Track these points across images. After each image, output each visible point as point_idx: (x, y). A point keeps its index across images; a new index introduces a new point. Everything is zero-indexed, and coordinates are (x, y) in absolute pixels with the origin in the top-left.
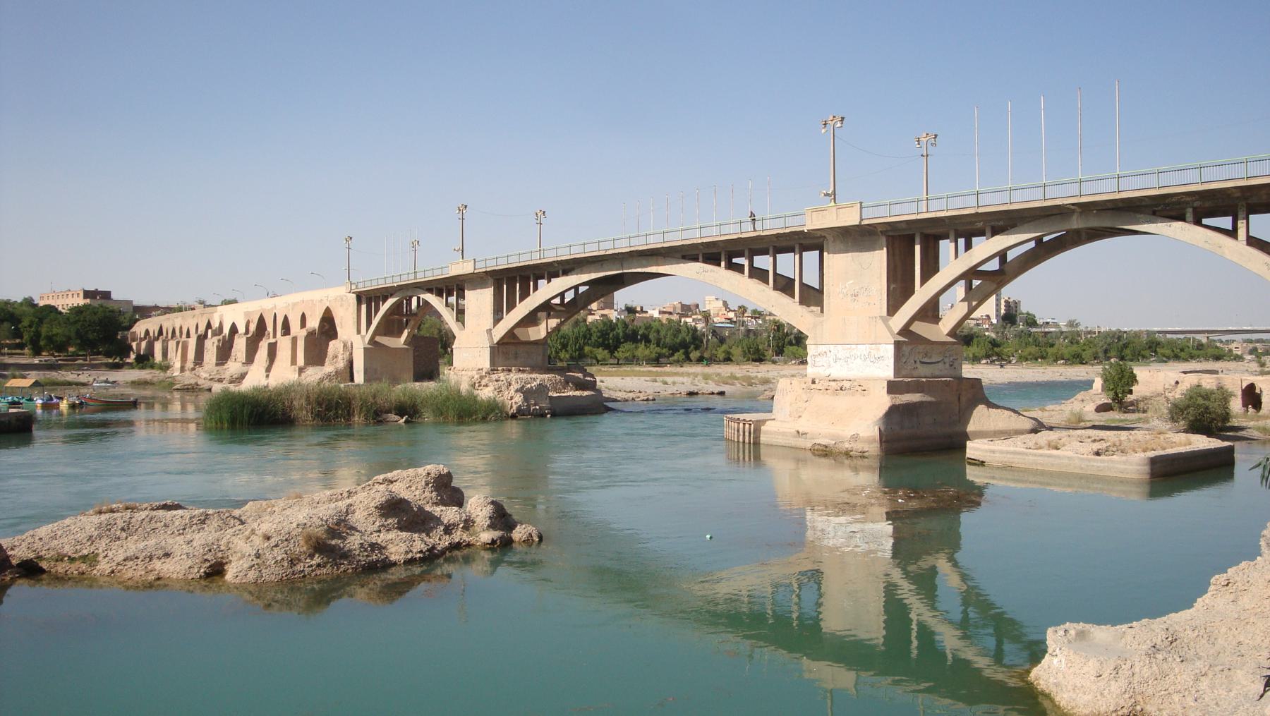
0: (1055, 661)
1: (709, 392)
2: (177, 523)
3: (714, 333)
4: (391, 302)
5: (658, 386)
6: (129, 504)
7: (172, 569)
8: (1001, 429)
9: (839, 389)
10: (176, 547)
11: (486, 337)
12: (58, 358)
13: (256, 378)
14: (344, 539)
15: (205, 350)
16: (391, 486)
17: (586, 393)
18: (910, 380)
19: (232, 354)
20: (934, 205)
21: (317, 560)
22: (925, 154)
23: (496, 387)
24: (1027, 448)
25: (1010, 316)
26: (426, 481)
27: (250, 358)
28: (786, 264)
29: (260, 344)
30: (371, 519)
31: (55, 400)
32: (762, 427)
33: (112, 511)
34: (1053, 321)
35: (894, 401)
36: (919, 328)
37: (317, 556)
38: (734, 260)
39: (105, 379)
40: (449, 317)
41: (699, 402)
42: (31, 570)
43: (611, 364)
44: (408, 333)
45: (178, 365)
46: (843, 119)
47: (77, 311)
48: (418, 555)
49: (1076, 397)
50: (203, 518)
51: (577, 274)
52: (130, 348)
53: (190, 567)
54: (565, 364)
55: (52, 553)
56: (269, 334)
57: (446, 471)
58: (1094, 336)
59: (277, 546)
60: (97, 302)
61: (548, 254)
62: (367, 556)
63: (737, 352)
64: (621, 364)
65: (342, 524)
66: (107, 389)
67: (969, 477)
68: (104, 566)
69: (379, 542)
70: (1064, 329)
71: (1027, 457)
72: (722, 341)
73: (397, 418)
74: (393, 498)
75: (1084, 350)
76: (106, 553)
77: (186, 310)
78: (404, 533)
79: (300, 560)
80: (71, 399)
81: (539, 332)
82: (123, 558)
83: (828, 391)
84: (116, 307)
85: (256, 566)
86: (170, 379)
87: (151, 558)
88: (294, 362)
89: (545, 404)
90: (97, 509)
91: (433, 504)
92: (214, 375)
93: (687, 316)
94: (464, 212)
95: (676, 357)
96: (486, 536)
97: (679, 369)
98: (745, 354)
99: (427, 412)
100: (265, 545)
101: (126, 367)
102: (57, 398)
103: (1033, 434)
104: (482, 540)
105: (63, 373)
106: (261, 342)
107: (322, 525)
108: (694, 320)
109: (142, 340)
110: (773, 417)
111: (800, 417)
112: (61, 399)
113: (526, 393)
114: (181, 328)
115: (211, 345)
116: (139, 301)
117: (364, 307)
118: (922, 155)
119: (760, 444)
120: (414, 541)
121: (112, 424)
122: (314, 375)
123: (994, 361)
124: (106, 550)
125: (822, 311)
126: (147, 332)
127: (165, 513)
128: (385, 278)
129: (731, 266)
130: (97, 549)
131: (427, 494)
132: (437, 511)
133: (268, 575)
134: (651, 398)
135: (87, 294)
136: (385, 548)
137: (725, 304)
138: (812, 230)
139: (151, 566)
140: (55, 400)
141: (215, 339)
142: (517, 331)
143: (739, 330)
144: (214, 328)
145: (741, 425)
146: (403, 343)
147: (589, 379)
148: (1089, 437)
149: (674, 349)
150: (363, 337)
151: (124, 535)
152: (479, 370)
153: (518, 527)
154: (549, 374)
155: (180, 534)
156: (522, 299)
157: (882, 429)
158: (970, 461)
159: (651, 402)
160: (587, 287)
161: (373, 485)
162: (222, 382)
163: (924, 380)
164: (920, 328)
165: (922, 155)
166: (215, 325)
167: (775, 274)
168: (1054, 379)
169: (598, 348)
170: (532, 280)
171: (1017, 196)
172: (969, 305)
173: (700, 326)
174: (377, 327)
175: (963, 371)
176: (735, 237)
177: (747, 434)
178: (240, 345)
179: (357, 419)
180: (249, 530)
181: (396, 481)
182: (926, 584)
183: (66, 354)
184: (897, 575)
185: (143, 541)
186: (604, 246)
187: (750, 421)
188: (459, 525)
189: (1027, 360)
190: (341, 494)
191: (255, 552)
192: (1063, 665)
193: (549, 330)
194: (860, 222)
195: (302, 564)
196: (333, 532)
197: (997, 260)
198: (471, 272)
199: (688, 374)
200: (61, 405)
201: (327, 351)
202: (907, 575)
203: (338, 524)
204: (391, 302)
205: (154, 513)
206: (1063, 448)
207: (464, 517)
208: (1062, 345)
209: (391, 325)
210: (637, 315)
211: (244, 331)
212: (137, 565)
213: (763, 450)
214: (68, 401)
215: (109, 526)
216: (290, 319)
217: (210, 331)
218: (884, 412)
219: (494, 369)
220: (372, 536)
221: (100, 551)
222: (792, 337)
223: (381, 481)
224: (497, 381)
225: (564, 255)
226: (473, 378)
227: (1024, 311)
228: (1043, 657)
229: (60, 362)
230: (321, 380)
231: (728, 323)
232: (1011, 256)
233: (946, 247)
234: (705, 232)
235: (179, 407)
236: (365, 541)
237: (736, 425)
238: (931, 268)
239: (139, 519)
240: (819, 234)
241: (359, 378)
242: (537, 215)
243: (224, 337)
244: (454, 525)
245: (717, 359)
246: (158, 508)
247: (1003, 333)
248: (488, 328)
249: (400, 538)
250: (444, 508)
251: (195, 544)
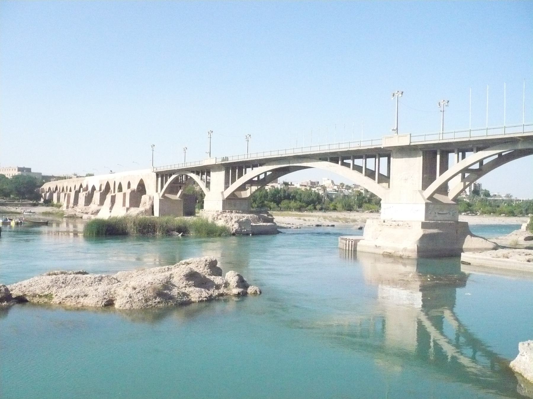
0: (523, 358)
1: (327, 225)
2: (88, 281)
3: (328, 196)
4: (173, 177)
5: (301, 222)
6: (62, 271)
7: (89, 302)
8: (478, 248)
9: (397, 225)
10: (90, 292)
11: (221, 195)
12: (5, 200)
13: (105, 214)
14: (170, 290)
15: (79, 198)
16: (188, 266)
17: (269, 224)
18: (433, 222)
19: (93, 200)
20: (445, 136)
21: (158, 300)
22: (442, 110)
23: (225, 220)
24: (492, 257)
25: (476, 192)
26: (205, 264)
27: (102, 203)
28: (371, 163)
29: (107, 196)
30: (182, 281)
31: (8, 221)
32: (358, 243)
33: (55, 274)
34: (499, 194)
35: (424, 232)
36: (437, 196)
37: (158, 298)
38: (345, 161)
39: (29, 211)
40: (202, 185)
41: (320, 230)
42: (21, 300)
43: (277, 210)
44: (182, 192)
45: (65, 205)
46: (402, 92)
47: (16, 177)
48: (204, 299)
49: (513, 232)
50: (100, 279)
51: (267, 166)
52: (42, 196)
53: (97, 302)
54: (255, 209)
55: (31, 293)
56: (111, 191)
57: (214, 259)
58: (520, 202)
59: (139, 292)
60: (25, 174)
61: (252, 156)
62: (181, 298)
63: (339, 206)
64: (282, 210)
65: (169, 283)
66: (30, 216)
67: (462, 270)
68: (56, 300)
69: (186, 292)
70: (505, 198)
71: (492, 262)
72: (332, 200)
73: (177, 233)
74: (192, 271)
75: (515, 209)
76: (56, 294)
77: (68, 178)
78: (197, 288)
79: (150, 300)
80: (16, 220)
81: (246, 194)
82: (65, 296)
83: (391, 226)
84: (34, 176)
85: (130, 302)
86: (62, 212)
87: (78, 297)
88: (124, 205)
89: (249, 229)
90: (48, 273)
91: (208, 275)
92: (84, 210)
93: (314, 187)
94: (211, 134)
95: (309, 208)
96: (236, 291)
97: (311, 213)
98: (343, 207)
99: (192, 231)
100: (134, 292)
101: (40, 205)
102: (10, 219)
103: (494, 251)
104: (233, 293)
105: (9, 207)
106: (108, 195)
107: (160, 283)
108: (317, 189)
109: (47, 192)
110: (363, 238)
111: (377, 238)
112: (11, 220)
113: (240, 223)
114: (67, 187)
115: (82, 196)
116: (45, 173)
117: (160, 179)
118: (441, 111)
119: (356, 251)
120: (202, 292)
121: (31, 232)
122: (134, 212)
123: (468, 214)
124: (56, 292)
125: (389, 187)
126: (50, 189)
127: (81, 276)
128: (171, 165)
129: (343, 164)
130: (52, 292)
131: (206, 270)
132: (212, 278)
133: (135, 306)
134: (299, 227)
135: (20, 169)
136: (189, 295)
137: (332, 182)
138: (385, 147)
139: (79, 300)
140: (8, 221)
141: (84, 193)
142: (235, 193)
143: (340, 195)
144: (83, 188)
145: (348, 242)
146: (178, 197)
147: (270, 217)
148: (524, 253)
149: (308, 204)
150: (159, 194)
151: (63, 285)
152: (217, 211)
153: (250, 286)
154: (251, 214)
155: (90, 286)
156: (238, 178)
157: (419, 246)
158: (463, 262)
159: (299, 229)
160: (271, 172)
161: (180, 265)
162: (88, 214)
163: (440, 222)
164: (438, 197)
165: (441, 111)
166: (84, 186)
167: (366, 169)
168: (500, 224)
169: (271, 202)
170: (244, 168)
171: (490, 132)
172: (465, 184)
173: (321, 192)
174: (166, 189)
175: (459, 218)
176: (346, 150)
177: (350, 246)
178: (97, 196)
179: (158, 234)
180: (125, 285)
181: (191, 263)
182: (438, 323)
183: (9, 198)
184: (423, 318)
185: (74, 288)
186: (281, 152)
187: (352, 240)
188: (222, 285)
189: (485, 213)
190: (165, 269)
191: (129, 295)
192: (528, 360)
193: (252, 193)
194: (410, 144)
195: (151, 301)
196: (165, 287)
197: (478, 164)
198: (214, 164)
199: (316, 216)
200: (11, 223)
201: (141, 200)
202: (430, 319)
203: (167, 282)
204: (173, 177)
205: (77, 275)
206: (511, 258)
207: (224, 282)
208: (504, 206)
209: (173, 188)
210: (289, 186)
211: (99, 189)
212: (72, 300)
213: (358, 254)
214: (15, 221)
215: (56, 281)
216: (122, 184)
217: (82, 189)
218: (420, 237)
219: (224, 211)
220: (182, 289)
221: (54, 293)
222: (367, 199)
223: (183, 263)
224: (226, 217)
225: (261, 156)
226: (214, 215)
227: (484, 189)
228: (516, 356)
229: (7, 202)
230: (138, 214)
231: (334, 191)
232: (485, 162)
233: (452, 157)
234: (322, 148)
235: (65, 225)
236: (180, 291)
237: (345, 241)
238: (444, 167)
239: (70, 278)
240: (389, 149)
241: (157, 214)
242: (246, 136)
243: (89, 192)
244: (220, 285)
245: (330, 209)
246: (77, 273)
247: (473, 199)
248: (222, 191)
249: (196, 290)
250: (215, 277)
251: (99, 290)
